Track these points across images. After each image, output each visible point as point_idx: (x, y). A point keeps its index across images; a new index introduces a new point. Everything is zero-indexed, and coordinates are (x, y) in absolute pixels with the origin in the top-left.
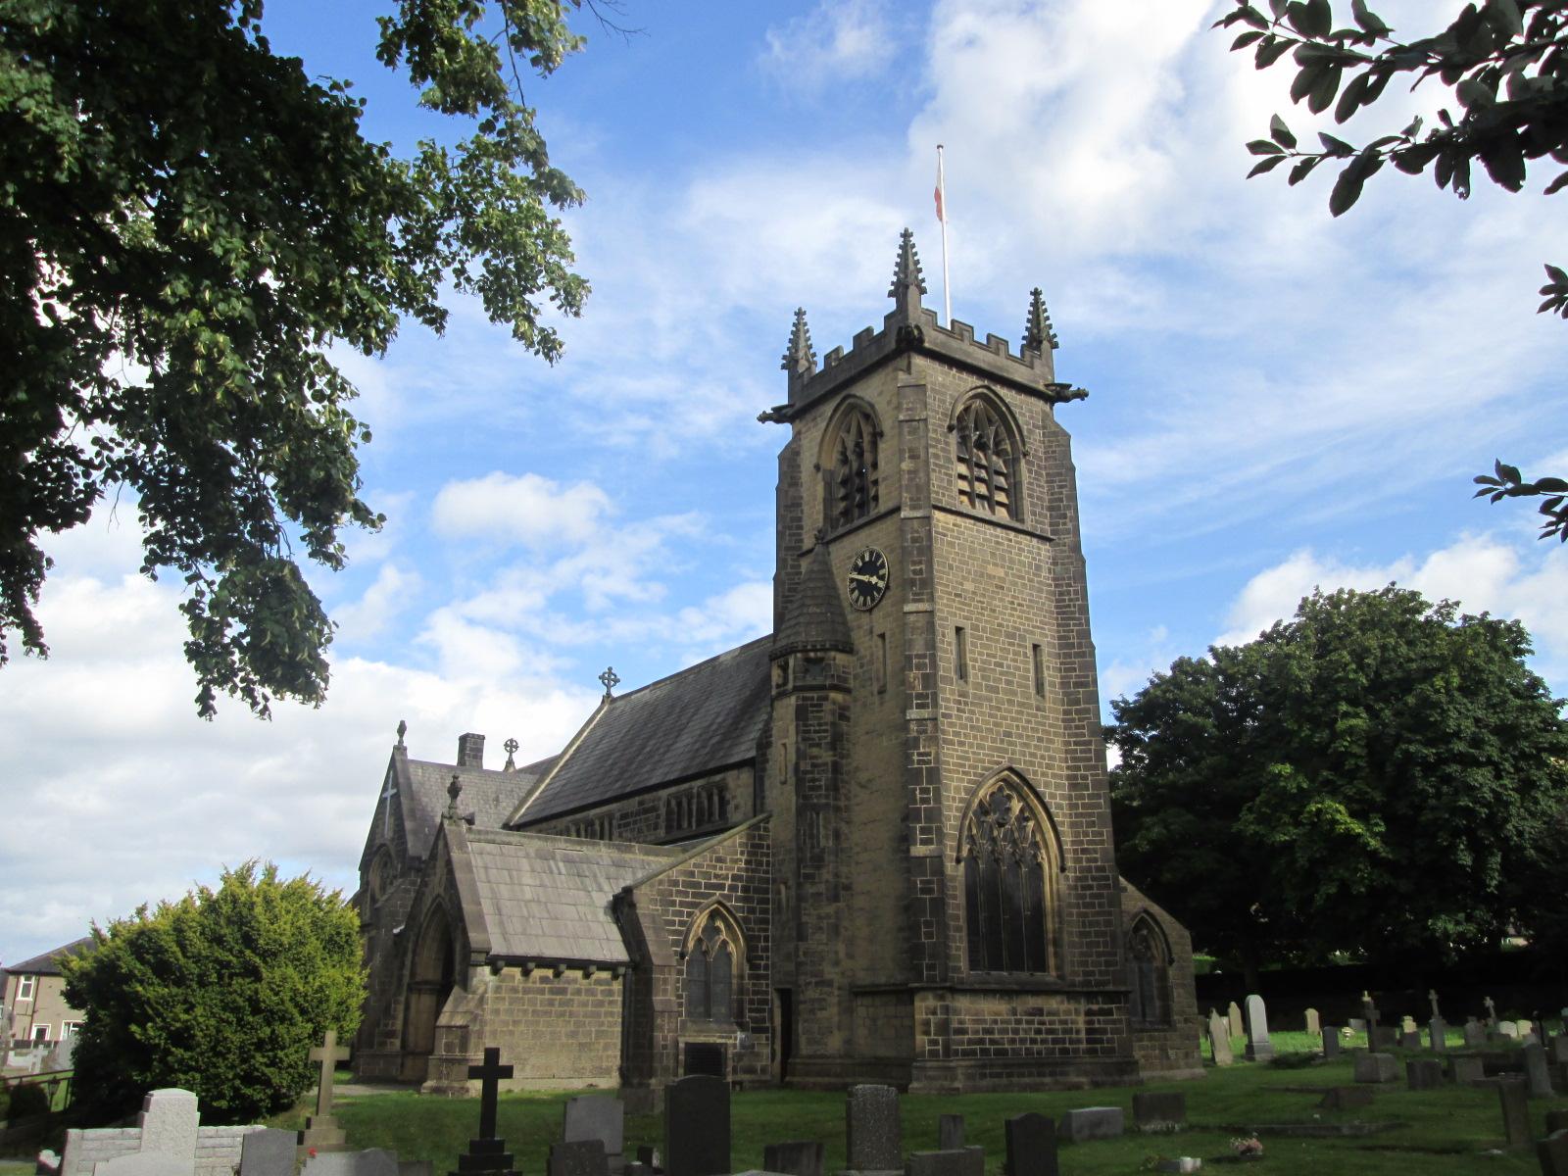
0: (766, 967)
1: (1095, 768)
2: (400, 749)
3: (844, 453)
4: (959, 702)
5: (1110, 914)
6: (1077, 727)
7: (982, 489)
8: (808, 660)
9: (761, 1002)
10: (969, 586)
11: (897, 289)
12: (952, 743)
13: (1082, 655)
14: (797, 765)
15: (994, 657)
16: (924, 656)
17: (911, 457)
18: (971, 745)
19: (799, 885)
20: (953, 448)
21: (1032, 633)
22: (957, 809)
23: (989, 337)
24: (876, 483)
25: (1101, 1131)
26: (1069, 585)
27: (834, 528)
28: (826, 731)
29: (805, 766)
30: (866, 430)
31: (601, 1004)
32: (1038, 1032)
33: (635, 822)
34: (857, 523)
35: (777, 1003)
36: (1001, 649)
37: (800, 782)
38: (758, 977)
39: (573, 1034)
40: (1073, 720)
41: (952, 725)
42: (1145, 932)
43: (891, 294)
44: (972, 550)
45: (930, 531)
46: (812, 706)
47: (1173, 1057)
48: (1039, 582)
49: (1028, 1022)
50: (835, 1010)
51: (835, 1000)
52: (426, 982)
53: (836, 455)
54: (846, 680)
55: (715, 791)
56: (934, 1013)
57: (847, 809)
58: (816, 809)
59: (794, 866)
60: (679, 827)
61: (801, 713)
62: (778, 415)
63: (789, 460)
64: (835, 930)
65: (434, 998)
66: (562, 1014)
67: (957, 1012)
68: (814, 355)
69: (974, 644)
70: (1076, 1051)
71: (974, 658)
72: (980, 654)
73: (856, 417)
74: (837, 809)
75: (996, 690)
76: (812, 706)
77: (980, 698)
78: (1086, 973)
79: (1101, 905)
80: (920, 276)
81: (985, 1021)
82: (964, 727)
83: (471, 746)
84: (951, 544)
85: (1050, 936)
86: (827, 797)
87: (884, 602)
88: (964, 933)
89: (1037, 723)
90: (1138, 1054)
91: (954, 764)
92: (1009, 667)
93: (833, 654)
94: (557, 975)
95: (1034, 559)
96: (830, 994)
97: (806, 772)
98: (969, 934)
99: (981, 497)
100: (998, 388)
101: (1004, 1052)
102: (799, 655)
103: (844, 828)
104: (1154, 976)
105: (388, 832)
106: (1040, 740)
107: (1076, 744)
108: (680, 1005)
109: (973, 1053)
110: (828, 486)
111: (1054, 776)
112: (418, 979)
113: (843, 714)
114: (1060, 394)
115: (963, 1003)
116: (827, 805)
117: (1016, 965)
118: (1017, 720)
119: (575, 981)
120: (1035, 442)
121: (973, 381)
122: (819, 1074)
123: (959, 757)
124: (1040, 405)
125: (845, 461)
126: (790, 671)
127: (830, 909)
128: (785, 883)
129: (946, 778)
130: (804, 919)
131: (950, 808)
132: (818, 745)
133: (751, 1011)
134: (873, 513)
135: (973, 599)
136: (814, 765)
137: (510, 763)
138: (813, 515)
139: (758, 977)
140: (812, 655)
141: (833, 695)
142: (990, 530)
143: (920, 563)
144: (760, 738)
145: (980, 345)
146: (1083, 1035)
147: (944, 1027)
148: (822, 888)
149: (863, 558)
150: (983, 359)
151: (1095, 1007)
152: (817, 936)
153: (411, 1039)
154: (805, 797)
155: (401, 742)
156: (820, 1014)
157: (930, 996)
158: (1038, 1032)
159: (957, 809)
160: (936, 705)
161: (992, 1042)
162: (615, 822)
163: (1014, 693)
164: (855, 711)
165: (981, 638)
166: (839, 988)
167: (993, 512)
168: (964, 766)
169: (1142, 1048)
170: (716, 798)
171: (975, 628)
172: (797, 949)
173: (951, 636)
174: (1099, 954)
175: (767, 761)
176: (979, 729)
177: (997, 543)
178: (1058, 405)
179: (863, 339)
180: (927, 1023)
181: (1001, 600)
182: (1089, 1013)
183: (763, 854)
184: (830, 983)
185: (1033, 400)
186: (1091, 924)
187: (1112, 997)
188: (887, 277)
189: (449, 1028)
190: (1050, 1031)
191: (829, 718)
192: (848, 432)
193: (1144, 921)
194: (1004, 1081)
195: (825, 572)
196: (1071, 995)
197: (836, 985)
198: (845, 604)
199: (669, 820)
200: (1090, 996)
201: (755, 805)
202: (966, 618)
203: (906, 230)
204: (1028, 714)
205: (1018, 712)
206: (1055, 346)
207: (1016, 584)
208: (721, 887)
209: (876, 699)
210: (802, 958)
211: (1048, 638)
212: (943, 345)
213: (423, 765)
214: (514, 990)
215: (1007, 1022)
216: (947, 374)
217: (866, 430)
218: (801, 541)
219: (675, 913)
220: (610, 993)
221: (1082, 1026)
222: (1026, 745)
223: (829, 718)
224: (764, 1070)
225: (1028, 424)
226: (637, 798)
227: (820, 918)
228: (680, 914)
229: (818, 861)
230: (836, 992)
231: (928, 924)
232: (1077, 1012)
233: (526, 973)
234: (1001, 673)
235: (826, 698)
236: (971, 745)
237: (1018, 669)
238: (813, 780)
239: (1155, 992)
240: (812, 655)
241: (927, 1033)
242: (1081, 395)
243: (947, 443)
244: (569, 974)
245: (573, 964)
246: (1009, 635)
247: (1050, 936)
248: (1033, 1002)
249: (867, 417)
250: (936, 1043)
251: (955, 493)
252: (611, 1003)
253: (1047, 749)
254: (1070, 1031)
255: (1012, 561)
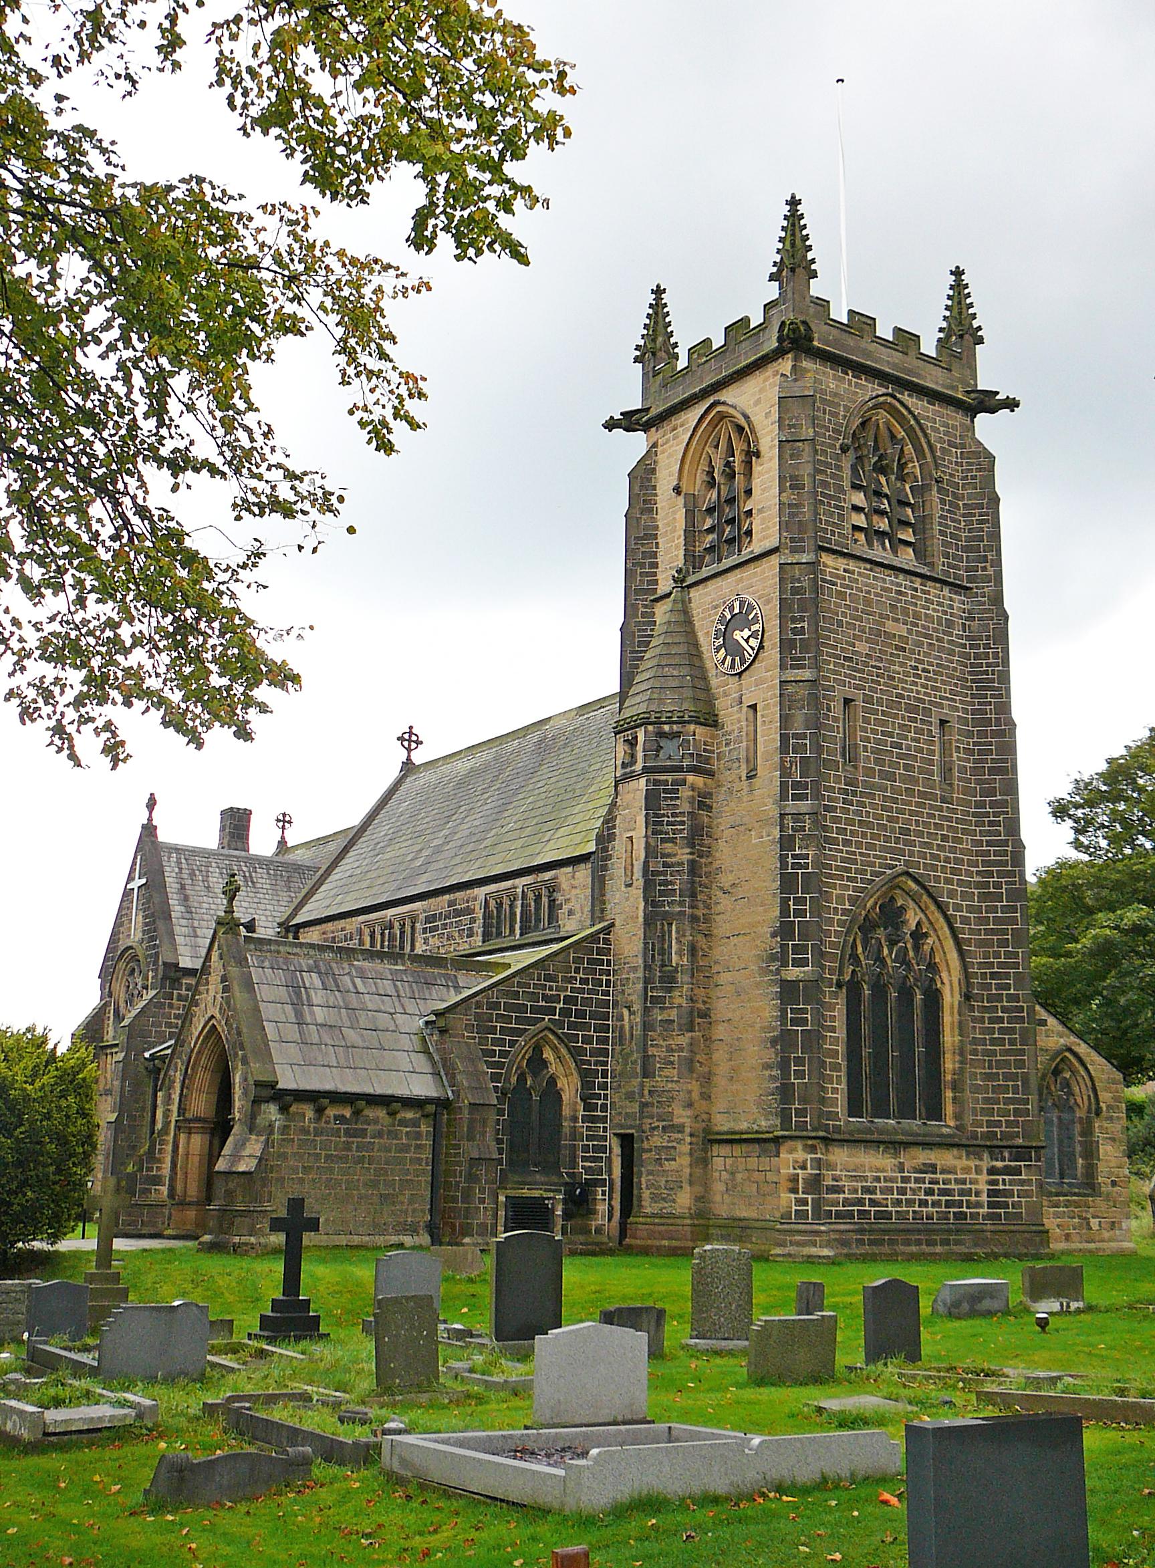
0: (604, 1106)
1: (1011, 874)
2: (149, 830)
3: (710, 473)
4: (846, 792)
5: (1022, 1052)
6: (991, 823)
7: (883, 525)
8: (662, 734)
9: (597, 1149)
10: (862, 647)
11: (780, 271)
12: (835, 842)
13: (1001, 734)
14: (646, 863)
15: (891, 735)
16: (804, 736)
17: (792, 487)
18: (859, 845)
19: (646, 1010)
20: (847, 473)
21: (940, 706)
22: (841, 923)
23: (898, 331)
24: (749, 513)
25: (986, 1304)
26: (987, 646)
27: (697, 567)
28: (683, 823)
29: (656, 865)
30: (739, 447)
31: (405, 1149)
32: (930, 1192)
33: (445, 926)
34: (727, 563)
35: (617, 1150)
36: (901, 726)
37: (648, 885)
38: (593, 1119)
39: (374, 1184)
40: (987, 815)
41: (836, 820)
42: (1067, 1075)
43: (772, 278)
44: (868, 602)
45: (815, 580)
46: (665, 791)
47: (1095, 1226)
48: (951, 642)
49: (917, 1180)
50: (686, 1160)
51: (686, 1148)
52: (198, 1119)
53: (701, 477)
54: (707, 760)
55: (544, 892)
56: (804, 1168)
57: (707, 919)
58: (668, 918)
59: (640, 986)
60: (499, 934)
61: (652, 800)
62: (629, 421)
63: (642, 478)
64: (690, 1064)
65: (207, 1137)
66: (361, 1160)
67: (831, 1166)
68: (676, 345)
69: (866, 720)
70: (974, 1216)
71: (867, 736)
72: (874, 732)
73: (726, 428)
74: (694, 919)
75: (891, 777)
76: (665, 791)
77: (872, 786)
78: (990, 1124)
79: (1012, 1042)
80: (810, 256)
81: (865, 1178)
82: (850, 822)
83: (236, 824)
84: (842, 595)
85: (949, 1077)
86: (681, 904)
87: (756, 665)
88: (843, 1074)
89: (941, 818)
90: (1050, 1223)
91: (838, 868)
92: (909, 748)
93: (692, 727)
94: (357, 1113)
95: (945, 613)
96: (679, 1141)
97: (655, 873)
98: (849, 1075)
99: (881, 534)
100: (905, 397)
101: (887, 1216)
102: (650, 728)
103: (702, 942)
104: (1077, 1128)
105: (135, 934)
106: (945, 838)
107: (989, 843)
108: (500, 1151)
109: (850, 1215)
110: (690, 514)
111: (960, 883)
112: (189, 1115)
113: (703, 802)
114: (989, 403)
115: (840, 1156)
116: (682, 913)
117: (906, 1112)
118: (917, 814)
119: (376, 1121)
120: (952, 466)
121: (872, 389)
122: (670, 1239)
123: (843, 860)
124: (959, 418)
125: (711, 483)
126: (640, 747)
127: (684, 1040)
128: (628, 1008)
129: (827, 884)
130: (651, 1051)
131: (830, 922)
132: (673, 840)
133: (584, 1159)
134: (746, 554)
135: (866, 664)
136: (665, 865)
137: (282, 842)
138: (671, 553)
139: (593, 1119)
140: (666, 728)
141: (691, 778)
142: (890, 579)
143: (802, 619)
144: (602, 829)
145: (884, 342)
146: (984, 1198)
147: (814, 1184)
148: (673, 1014)
149: (731, 608)
150: (886, 361)
151: (999, 1164)
152: (666, 1072)
153: (179, 1188)
154: (654, 904)
155: (150, 819)
156: (668, 1165)
157: (799, 1145)
158: (930, 1192)
159: (841, 923)
160: (817, 796)
161: (873, 1203)
162: (418, 925)
163: (915, 781)
164: (720, 797)
165: (876, 712)
166: (691, 1135)
167: (895, 552)
168: (848, 870)
169: (1056, 1215)
170: (545, 900)
171: (868, 700)
172: (642, 1085)
173: (837, 709)
174: (1008, 1101)
175: (610, 857)
176: (869, 825)
177: (899, 593)
178: (981, 419)
179: (738, 329)
180: (794, 1179)
181: (902, 665)
182: (992, 1171)
183: (602, 972)
184: (680, 1129)
185: (949, 411)
186: (999, 1064)
187: (1021, 1153)
188: (769, 253)
189: (229, 1173)
190: (943, 1192)
191: (686, 807)
192: (717, 447)
193: (1061, 1063)
194: (886, 1249)
195: (685, 621)
196: (971, 1147)
197: (688, 1130)
198: (709, 664)
199: (486, 926)
200: (994, 1150)
201: (592, 911)
202: (857, 687)
203: (793, 197)
204: (931, 807)
205: (918, 804)
206: (980, 341)
207: (920, 644)
208: (552, 1011)
209: (745, 784)
210: (647, 1098)
211: (956, 711)
212: (836, 343)
213: (177, 850)
214: (305, 1131)
215: (892, 1180)
216: (842, 380)
217: (739, 447)
218: (656, 582)
219: (495, 1042)
220: (418, 1136)
221: (984, 1187)
222: (928, 845)
223: (686, 807)
224: (599, 1230)
225: (941, 440)
226: (447, 897)
227: (670, 1050)
228: (501, 1042)
229: (669, 980)
230: (688, 1139)
231: (799, 1061)
232: (978, 1170)
233: (320, 1111)
234: (899, 756)
235: (684, 783)
236: (859, 845)
237: (921, 750)
238: (666, 883)
239: (1078, 1148)
240: (666, 728)
241: (794, 1190)
242: (1011, 404)
243: (839, 468)
244: (370, 1113)
245: (374, 1100)
246: (910, 708)
247: (949, 1077)
248: (924, 1157)
249: (740, 429)
250: (804, 1202)
251: (847, 530)
252: (418, 1147)
253: (953, 850)
254: (968, 1192)
255: (917, 615)
